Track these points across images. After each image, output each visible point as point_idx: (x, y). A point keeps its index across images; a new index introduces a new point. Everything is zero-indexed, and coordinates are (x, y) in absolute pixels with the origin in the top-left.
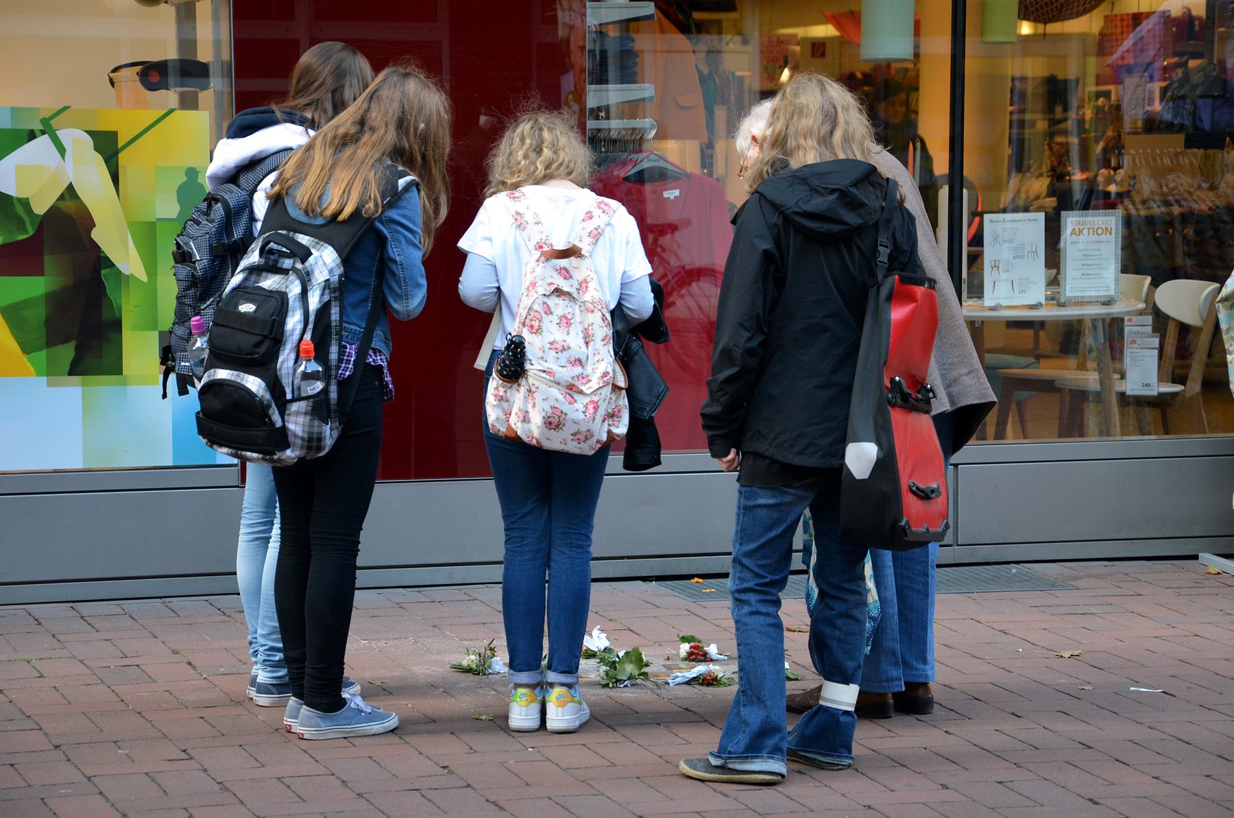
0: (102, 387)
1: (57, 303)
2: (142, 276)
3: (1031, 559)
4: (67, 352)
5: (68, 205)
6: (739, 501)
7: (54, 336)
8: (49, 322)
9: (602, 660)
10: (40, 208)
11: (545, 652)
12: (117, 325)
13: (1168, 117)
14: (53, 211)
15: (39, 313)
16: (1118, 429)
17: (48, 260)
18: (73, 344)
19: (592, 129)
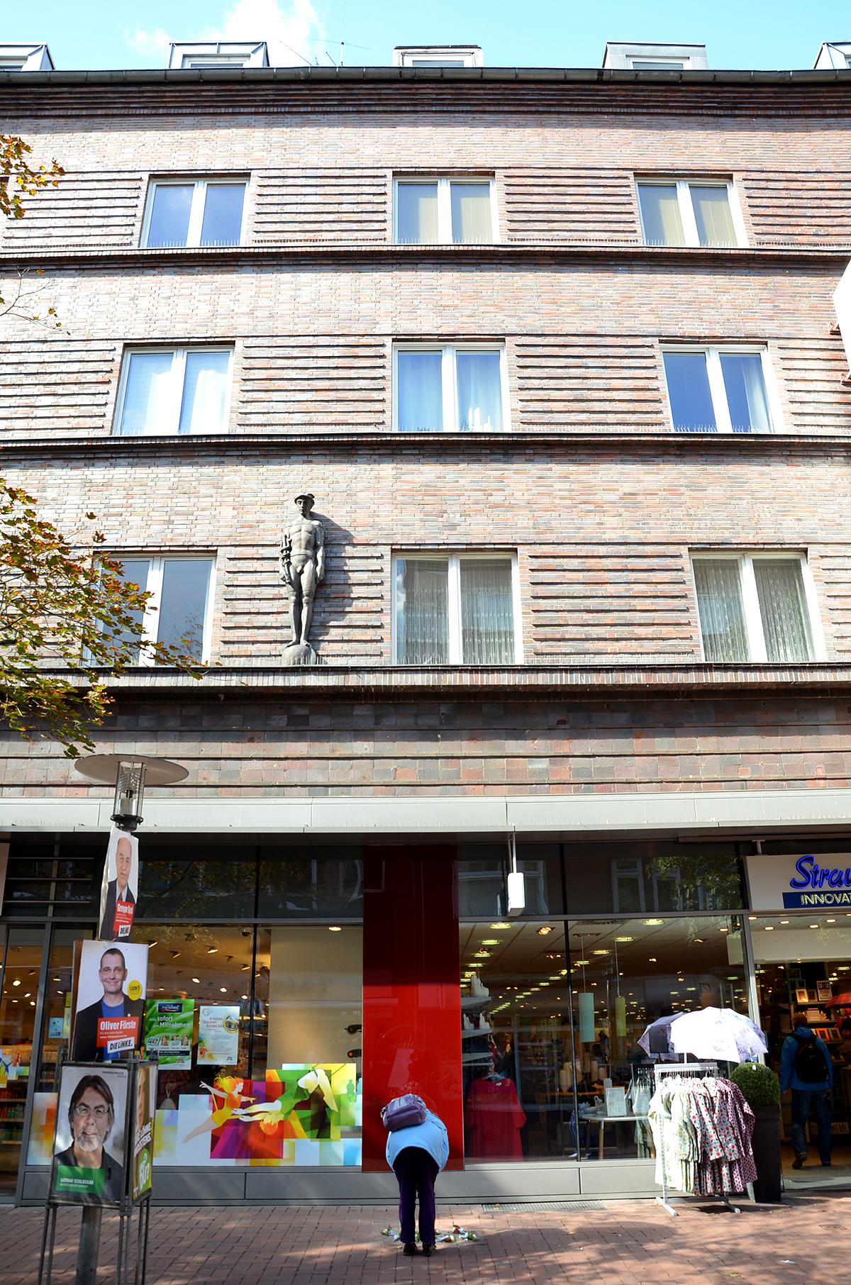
0: (325, 1142)
1: (314, 1118)
2: (337, 1110)
3: (648, 189)
4: (316, 1132)
5: (318, 1091)
6: (747, 1000)
7: (312, 1128)
8: (311, 1123)
9: (249, 1077)
10: (311, 1092)
11: (417, 1229)
12: (329, 1124)
13: (58, 1189)
14: (314, 1092)
15: (309, 1120)
16: (145, 896)
17: (312, 1106)
18: (317, 1130)
19: (826, 770)
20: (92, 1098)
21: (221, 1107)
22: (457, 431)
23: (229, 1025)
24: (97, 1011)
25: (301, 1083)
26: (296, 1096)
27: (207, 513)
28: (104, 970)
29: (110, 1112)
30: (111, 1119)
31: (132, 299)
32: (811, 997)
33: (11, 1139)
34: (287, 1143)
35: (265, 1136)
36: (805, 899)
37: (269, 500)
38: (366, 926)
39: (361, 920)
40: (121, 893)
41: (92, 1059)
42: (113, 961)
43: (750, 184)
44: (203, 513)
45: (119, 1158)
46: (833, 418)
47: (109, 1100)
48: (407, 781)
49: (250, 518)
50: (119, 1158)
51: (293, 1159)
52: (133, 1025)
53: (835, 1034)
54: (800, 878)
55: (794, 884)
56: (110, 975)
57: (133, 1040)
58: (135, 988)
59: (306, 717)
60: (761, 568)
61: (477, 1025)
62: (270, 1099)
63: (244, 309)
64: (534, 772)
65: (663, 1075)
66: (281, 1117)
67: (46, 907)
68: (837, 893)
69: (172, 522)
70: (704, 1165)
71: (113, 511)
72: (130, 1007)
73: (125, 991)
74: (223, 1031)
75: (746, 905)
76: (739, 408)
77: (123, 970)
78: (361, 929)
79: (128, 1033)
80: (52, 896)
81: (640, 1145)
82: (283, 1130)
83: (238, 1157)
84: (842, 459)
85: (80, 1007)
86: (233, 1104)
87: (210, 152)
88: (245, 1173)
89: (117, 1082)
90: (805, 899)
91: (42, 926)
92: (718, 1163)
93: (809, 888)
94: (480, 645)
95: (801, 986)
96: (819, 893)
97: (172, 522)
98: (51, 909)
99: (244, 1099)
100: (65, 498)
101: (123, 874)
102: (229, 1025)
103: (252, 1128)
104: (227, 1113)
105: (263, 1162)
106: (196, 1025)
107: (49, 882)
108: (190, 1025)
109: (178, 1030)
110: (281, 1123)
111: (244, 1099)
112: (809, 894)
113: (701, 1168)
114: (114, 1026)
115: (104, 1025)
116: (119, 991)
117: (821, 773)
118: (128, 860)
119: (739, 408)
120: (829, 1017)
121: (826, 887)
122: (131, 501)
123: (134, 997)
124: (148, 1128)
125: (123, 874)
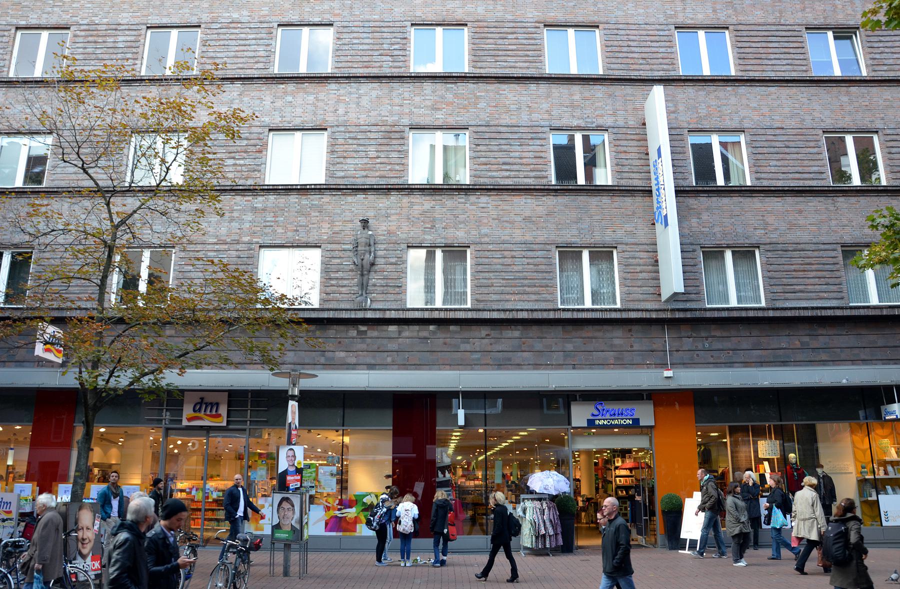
20: (286, 505)
21: (329, 510)
22: (466, 69)
23: (332, 475)
24: (285, 473)
25: (365, 500)
26: (362, 506)
27: (315, 226)
28: (288, 456)
29: (293, 510)
30: (294, 513)
31: (272, 103)
32: (623, 462)
33: (219, 526)
34: (358, 526)
35: (348, 523)
36: (597, 422)
37: (347, 219)
38: (394, 430)
39: (391, 428)
40: (293, 426)
41: (284, 490)
42: (291, 453)
43: (609, 32)
44: (313, 226)
45: (298, 527)
46: (638, 174)
47: (293, 506)
48: (413, 363)
49: (336, 229)
50: (298, 527)
51: (361, 533)
52: (299, 477)
53: (632, 481)
54: (596, 413)
55: (593, 415)
56: (290, 458)
57: (299, 483)
58: (299, 463)
59: (366, 331)
60: (593, 257)
61: (444, 476)
62: (351, 507)
63: (331, 109)
64: (473, 360)
65: (524, 499)
66: (356, 515)
67: (246, 421)
68: (613, 420)
69: (298, 231)
70: (539, 537)
71: (268, 224)
72: (299, 471)
73: (296, 465)
74: (330, 478)
75: (569, 423)
76: (589, 176)
77: (294, 456)
78: (391, 432)
79: (297, 480)
80: (249, 417)
81: (550, 536)
82: (356, 520)
83: (337, 531)
84: (640, 198)
85: (280, 471)
86: (334, 509)
87: (310, 10)
88: (340, 538)
89: (296, 500)
90: (597, 422)
91: (245, 430)
92: (544, 536)
93: (600, 417)
94: (451, 293)
95: (618, 456)
96: (604, 420)
97: (298, 231)
98: (248, 422)
99: (339, 507)
100: (243, 217)
101: (293, 419)
102: (332, 475)
103: (343, 519)
104: (332, 513)
105: (348, 534)
106: (317, 475)
107: (247, 410)
108: (314, 475)
109: (309, 477)
110: (356, 517)
111: (339, 507)
112: (599, 420)
113: (537, 538)
114: (292, 478)
115: (289, 478)
116: (294, 465)
117: (612, 362)
118: (295, 412)
119: (589, 176)
120: (631, 472)
121: (608, 416)
122: (277, 219)
123: (299, 467)
124: (306, 516)
125: (293, 419)
